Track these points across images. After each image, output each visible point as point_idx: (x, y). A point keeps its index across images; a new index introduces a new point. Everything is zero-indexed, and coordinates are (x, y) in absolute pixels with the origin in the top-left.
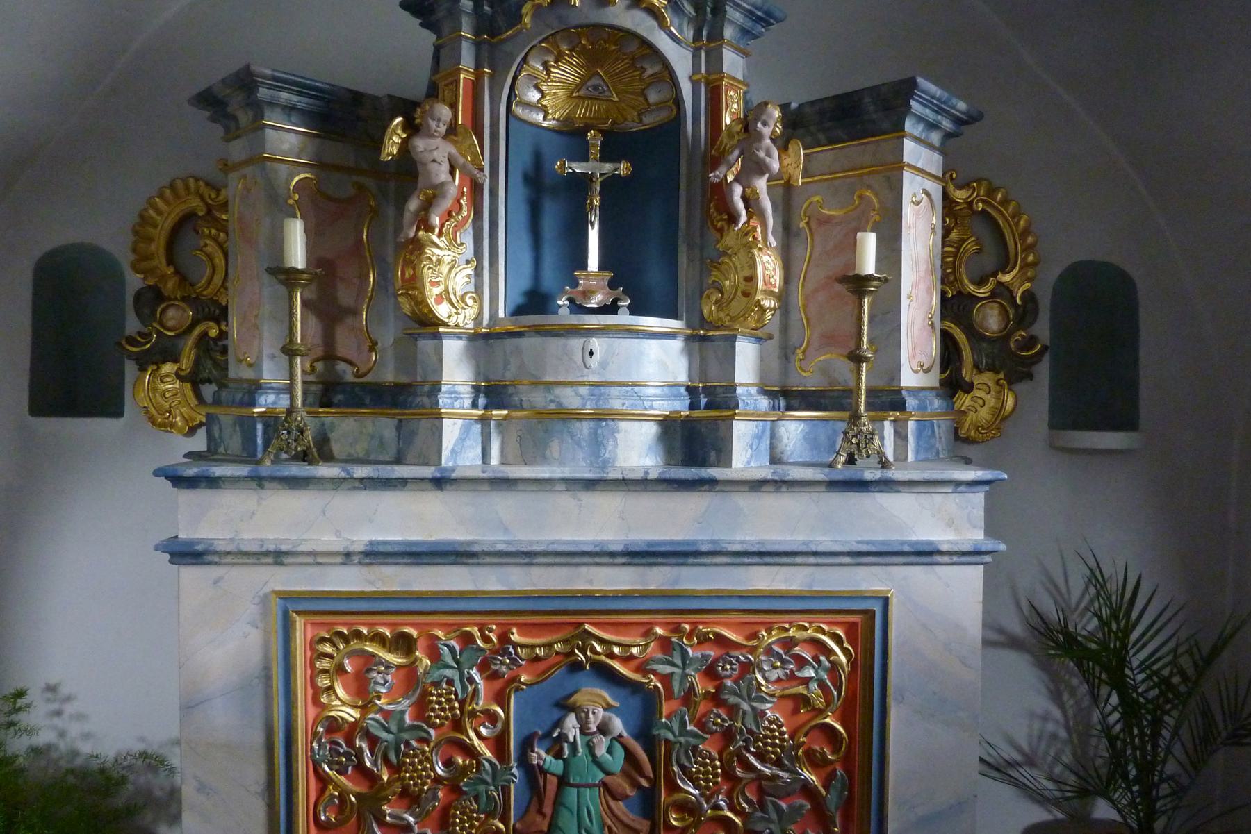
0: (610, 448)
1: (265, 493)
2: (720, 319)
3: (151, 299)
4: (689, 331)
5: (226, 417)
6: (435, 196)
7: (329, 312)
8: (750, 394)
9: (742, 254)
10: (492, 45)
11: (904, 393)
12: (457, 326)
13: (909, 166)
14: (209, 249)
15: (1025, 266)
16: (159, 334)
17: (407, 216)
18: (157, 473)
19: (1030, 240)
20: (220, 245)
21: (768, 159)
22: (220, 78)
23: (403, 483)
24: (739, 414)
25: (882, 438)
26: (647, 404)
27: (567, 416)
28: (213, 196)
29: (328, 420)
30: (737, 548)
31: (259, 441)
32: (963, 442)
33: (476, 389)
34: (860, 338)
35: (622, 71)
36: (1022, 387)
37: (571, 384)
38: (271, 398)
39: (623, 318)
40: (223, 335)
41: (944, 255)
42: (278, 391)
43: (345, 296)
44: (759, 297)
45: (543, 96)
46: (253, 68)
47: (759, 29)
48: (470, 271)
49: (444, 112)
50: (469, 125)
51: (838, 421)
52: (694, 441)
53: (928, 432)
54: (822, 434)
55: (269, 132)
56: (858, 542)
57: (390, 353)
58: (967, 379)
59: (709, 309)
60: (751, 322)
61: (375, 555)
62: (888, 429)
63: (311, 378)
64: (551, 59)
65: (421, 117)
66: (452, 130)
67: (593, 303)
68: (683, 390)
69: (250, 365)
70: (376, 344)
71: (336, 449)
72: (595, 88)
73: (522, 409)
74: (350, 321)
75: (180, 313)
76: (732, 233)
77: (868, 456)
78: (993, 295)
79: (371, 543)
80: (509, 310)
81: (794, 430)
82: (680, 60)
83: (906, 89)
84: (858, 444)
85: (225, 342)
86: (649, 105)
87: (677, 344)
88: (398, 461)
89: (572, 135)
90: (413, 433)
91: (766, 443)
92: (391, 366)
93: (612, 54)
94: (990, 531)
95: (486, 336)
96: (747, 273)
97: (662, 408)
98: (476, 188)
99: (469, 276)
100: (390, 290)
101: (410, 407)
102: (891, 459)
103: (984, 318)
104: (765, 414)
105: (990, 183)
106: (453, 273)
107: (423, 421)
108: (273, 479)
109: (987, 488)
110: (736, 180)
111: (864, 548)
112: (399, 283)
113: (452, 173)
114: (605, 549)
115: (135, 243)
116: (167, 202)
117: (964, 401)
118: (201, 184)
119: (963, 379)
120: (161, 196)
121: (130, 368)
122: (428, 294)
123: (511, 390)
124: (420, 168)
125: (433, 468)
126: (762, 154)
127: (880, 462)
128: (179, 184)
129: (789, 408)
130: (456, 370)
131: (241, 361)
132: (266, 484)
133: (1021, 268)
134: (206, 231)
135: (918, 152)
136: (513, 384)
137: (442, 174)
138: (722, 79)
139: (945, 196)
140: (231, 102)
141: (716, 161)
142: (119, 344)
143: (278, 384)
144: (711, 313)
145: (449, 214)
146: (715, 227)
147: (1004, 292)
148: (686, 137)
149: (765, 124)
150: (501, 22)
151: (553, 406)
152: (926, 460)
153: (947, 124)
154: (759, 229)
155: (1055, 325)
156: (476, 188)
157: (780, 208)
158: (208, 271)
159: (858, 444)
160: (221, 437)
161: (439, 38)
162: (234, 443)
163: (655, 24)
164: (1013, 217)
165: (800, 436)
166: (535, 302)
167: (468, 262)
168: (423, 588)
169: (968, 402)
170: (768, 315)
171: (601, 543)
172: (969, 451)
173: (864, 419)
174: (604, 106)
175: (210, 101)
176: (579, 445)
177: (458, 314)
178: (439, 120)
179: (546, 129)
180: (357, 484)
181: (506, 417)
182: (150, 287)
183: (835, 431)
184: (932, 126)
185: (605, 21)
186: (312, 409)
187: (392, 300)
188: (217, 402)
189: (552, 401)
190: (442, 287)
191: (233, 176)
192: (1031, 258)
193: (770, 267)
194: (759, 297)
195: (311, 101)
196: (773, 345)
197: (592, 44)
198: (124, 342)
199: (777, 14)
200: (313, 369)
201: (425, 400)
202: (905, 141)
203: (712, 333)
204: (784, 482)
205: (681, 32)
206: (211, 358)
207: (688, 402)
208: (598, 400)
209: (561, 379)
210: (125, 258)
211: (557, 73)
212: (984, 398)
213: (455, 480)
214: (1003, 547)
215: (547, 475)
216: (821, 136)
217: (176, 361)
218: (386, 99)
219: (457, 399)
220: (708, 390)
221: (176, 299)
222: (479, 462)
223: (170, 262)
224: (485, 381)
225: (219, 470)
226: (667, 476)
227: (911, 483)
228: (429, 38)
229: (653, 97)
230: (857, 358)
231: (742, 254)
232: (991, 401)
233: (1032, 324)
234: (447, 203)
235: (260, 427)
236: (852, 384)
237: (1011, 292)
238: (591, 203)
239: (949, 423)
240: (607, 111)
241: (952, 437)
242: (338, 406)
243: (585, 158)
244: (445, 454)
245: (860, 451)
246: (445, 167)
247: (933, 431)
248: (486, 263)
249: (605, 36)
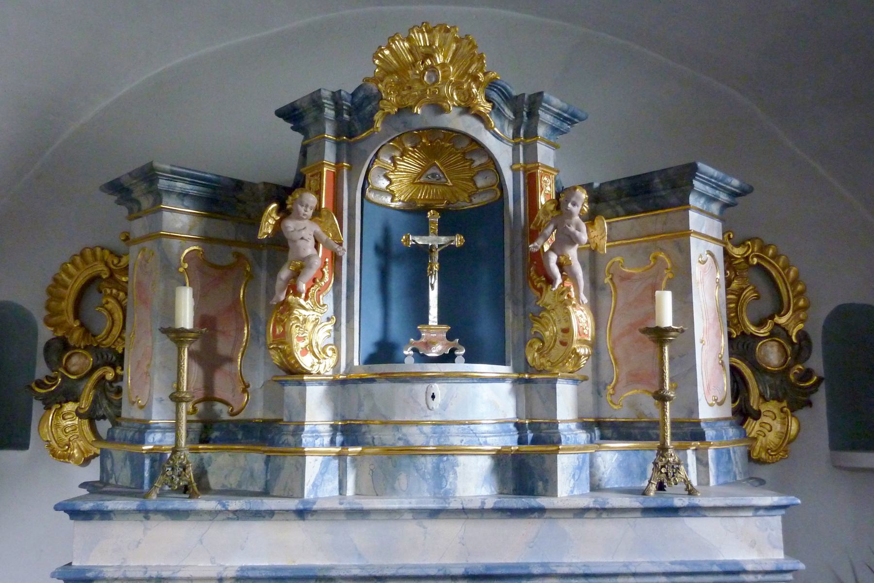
0: (451, 480)
1: (150, 524)
2: (542, 364)
3: (60, 348)
4: (516, 375)
5: (118, 452)
6: (302, 267)
7: (210, 361)
8: (571, 430)
9: (559, 310)
10: (349, 144)
11: (703, 425)
12: (319, 374)
13: (696, 233)
14: (109, 306)
15: (797, 309)
16: (64, 377)
17: (279, 284)
18: (57, 508)
19: (800, 288)
20: (119, 302)
21: (578, 233)
22: (129, 170)
23: (270, 514)
24: (563, 449)
25: (686, 466)
26: (482, 440)
27: (412, 452)
28: (116, 261)
29: (206, 456)
30: (565, 570)
31: (146, 474)
32: (757, 465)
33: (334, 428)
34: (662, 381)
35: (455, 163)
36: (803, 413)
37: (416, 423)
38: (158, 436)
39: (460, 366)
40: (118, 378)
41: (729, 302)
42: (164, 430)
43: (223, 347)
44: (575, 346)
45: (391, 183)
46: (156, 164)
47: (566, 126)
48: (330, 327)
49: (311, 199)
50: (330, 208)
51: (647, 450)
52: (523, 472)
53: (725, 458)
54: (634, 461)
55: (166, 214)
56: (672, 563)
57: (260, 394)
58: (755, 407)
59: (532, 356)
60: (569, 366)
62: (691, 457)
63: (193, 417)
64: (397, 154)
65: (292, 204)
66: (317, 212)
67: (434, 353)
68: (512, 426)
69: (141, 407)
70: (248, 386)
71: (214, 481)
72: (433, 175)
73: (374, 446)
74: (227, 367)
75: (82, 360)
76: (550, 292)
77: (676, 484)
78: (772, 335)
79: (242, 569)
80: (363, 358)
81: (610, 458)
82: (503, 153)
83: (690, 171)
84: (667, 474)
85: (119, 384)
86: (478, 189)
87: (506, 386)
88: (266, 493)
89: (415, 214)
90: (279, 469)
91: (586, 473)
92: (261, 404)
93: (445, 149)
94: (789, 550)
95: (343, 382)
96: (564, 325)
97: (496, 443)
98: (336, 259)
99: (329, 331)
100: (262, 339)
101: (278, 445)
102: (695, 483)
103: (765, 355)
104: (585, 448)
105: (762, 241)
106: (316, 329)
107: (289, 458)
108: (157, 511)
109: (783, 512)
110: (552, 249)
111: (678, 568)
112: (270, 339)
113: (317, 247)
114: (448, 573)
115: (49, 301)
116: (77, 268)
117: (753, 427)
118: (107, 252)
119: (751, 407)
120: (73, 263)
121: (37, 407)
122: (295, 348)
123: (364, 429)
124: (290, 244)
125: (297, 501)
126: (572, 229)
127: (687, 489)
128: (88, 252)
129: (603, 437)
130: (317, 411)
131: (134, 403)
132: (151, 516)
133: (794, 312)
134: (109, 291)
135: (702, 222)
136: (366, 423)
137: (308, 248)
138: (537, 168)
139: (726, 253)
140: (134, 191)
141: (534, 235)
142: (30, 387)
143: (161, 414)
144: (534, 359)
145: (314, 280)
146: (535, 287)
147: (779, 332)
148: (510, 218)
149: (574, 204)
150: (357, 126)
151: (401, 444)
152: (726, 484)
153: (724, 197)
154: (572, 289)
155: (827, 359)
156: (336, 259)
157: (588, 266)
158: (109, 324)
159: (667, 474)
160: (112, 470)
161: (306, 137)
162: (124, 476)
163: (482, 126)
164: (784, 269)
165: (615, 465)
166: (384, 352)
167: (328, 319)
169: (757, 427)
170: (583, 360)
171: (444, 567)
172: (763, 472)
173: (670, 451)
174: (440, 189)
175: (118, 189)
176: (424, 479)
177: (319, 363)
178: (307, 206)
179: (394, 209)
180: (231, 515)
181: (360, 453)
182: (58, 338)
183: (645, 460)
184: (712, 199)
185: (444, 125)
186: (195, 446)
187: (263, 348)
188: (111, 439)
189: (400, 439)
190: (307, 341)
191: (134, 249)
192: (801, 303)
193: (583, 320)
194: (575, 346)
195: (201, 188)
196: (588, 386)
197: (431, 142)
198: (33, 385)
199: (580, 114)
200: (194, 409)
201: (291, 439)
202: (691, 213)
203: (535, 377)
204: (604, 509)
205: (503, 131)
206: (107, 398)
207: (517, 437)
208: (440, 437)
209: (407, 419)
210: (39, 314)
211: (402, 165)
212: (772, 424)
213: (316, 511)
214: (802, 566)
215: (396, 506)
216: (620, 209)
217: (76, 400)
218: (261, 187)
219: (317, 437)
220: (534, 426)
221: (80, 348)
222: (336, 493)
223: (77, 316)
224: (342, 421)
225: (111, 504)
226: (501, 505)
227: (715, 509)
228: (298, 137)
229: (481, 182)
230: (661, 398)
231: (559, 310)
232: (777, 426)
233: (807, 358)
234: (311, 273)
235: (147, 462)
236: (657, 416)
237: (787, 332)
238: (431, 269)
239: (742, 449)
240: (443, 194)
241: (746, 460)
242: (215, 442)
243: (425, 232)
244: (307, 487)
245: (669, 480)
246: (312, 242)
247: (730, 458)
248: (344, 320)
249: (442, 136)
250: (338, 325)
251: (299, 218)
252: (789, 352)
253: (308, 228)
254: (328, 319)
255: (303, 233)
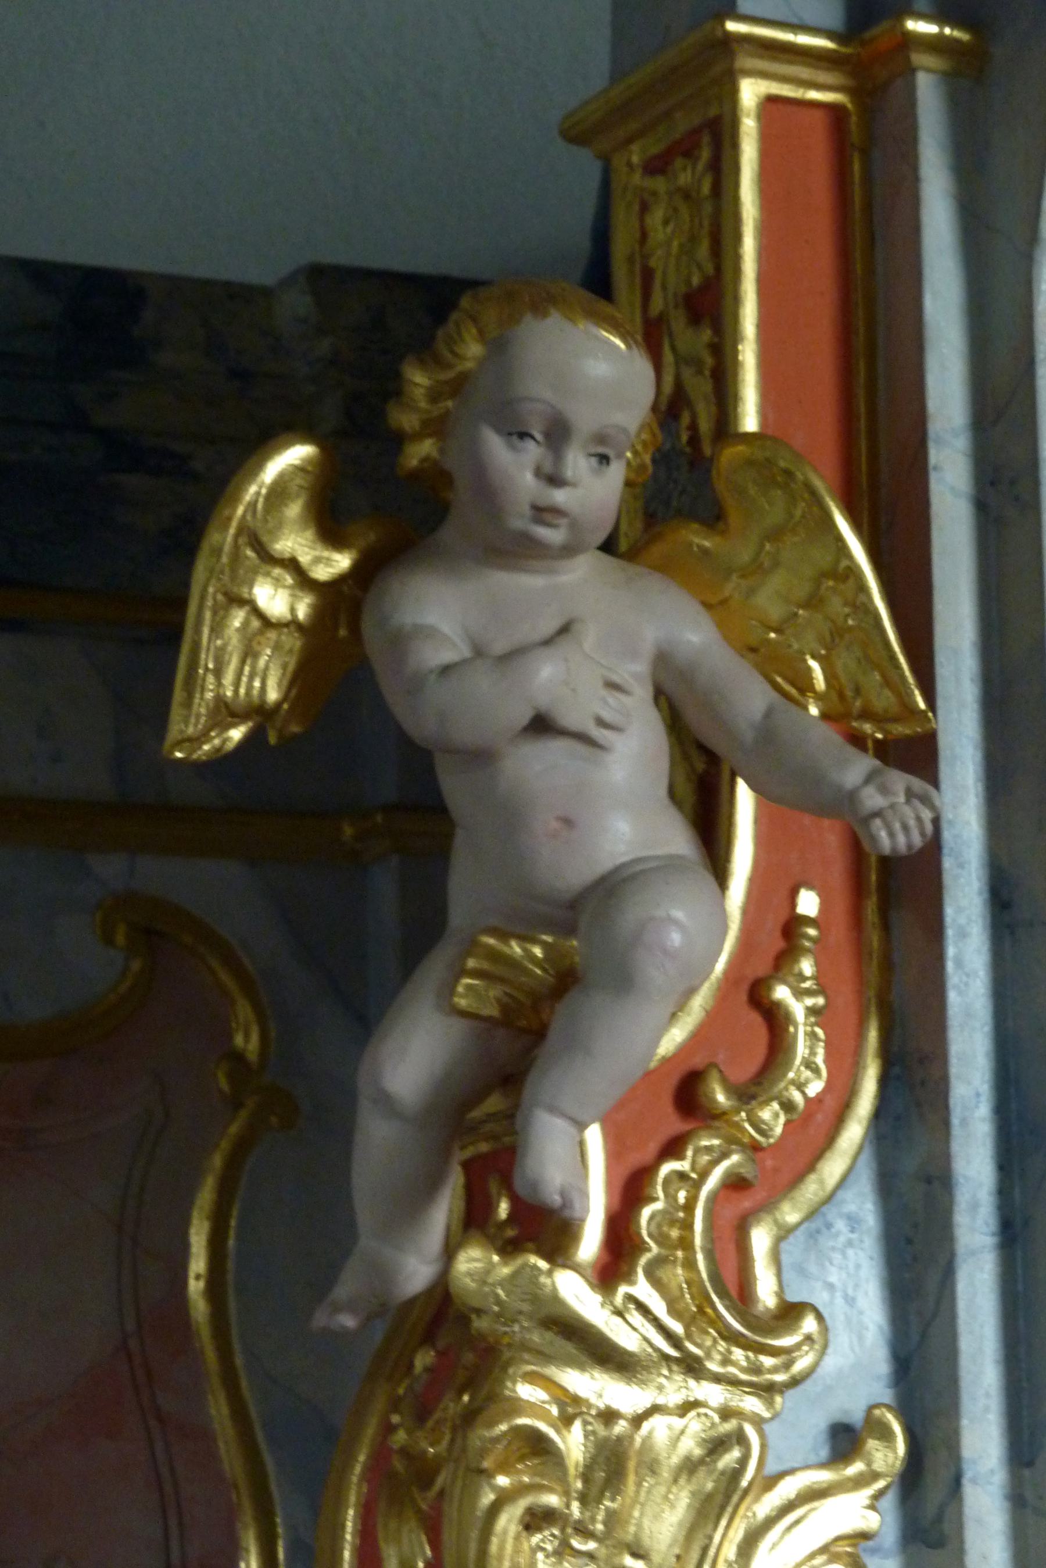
6: (565, 980)
17: (379, 1145)
49: (598, 371)
65: (436, 427)
124: (455, 788)
137: (614, 806)
167: (844, 1441)
178: (558, 433)
218: (298, 304)
246: (635, 758)
250: (934, 1494)
251: (516, 550)
252: (738, 1533)
253: (590, 637)
254: (844, 1441)
255: (547, 678)
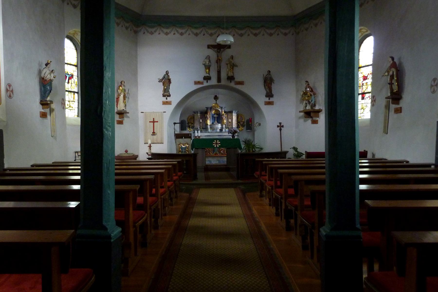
52: (221, 130)
61: (206, 136)
130: (209, 127)
166: (213, 123)
168: (187, 14)
